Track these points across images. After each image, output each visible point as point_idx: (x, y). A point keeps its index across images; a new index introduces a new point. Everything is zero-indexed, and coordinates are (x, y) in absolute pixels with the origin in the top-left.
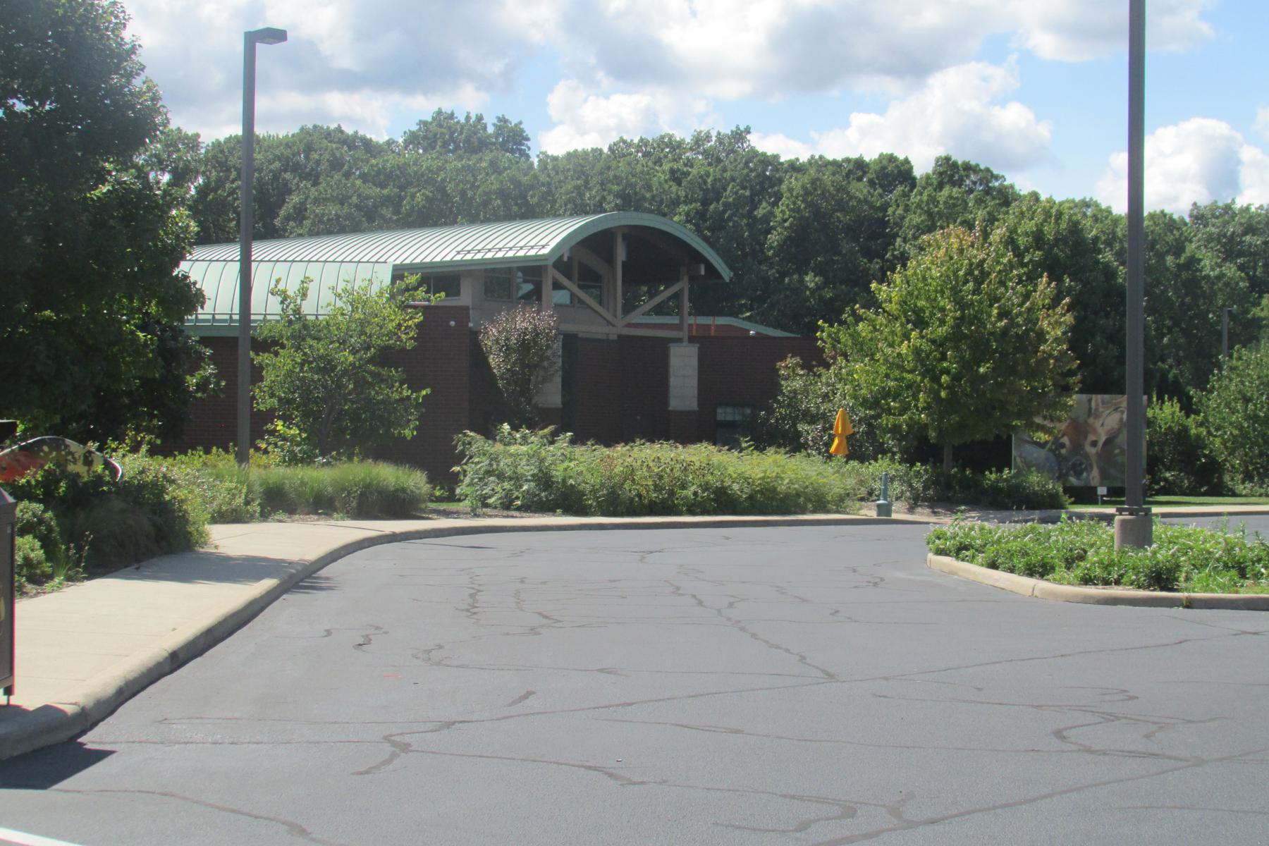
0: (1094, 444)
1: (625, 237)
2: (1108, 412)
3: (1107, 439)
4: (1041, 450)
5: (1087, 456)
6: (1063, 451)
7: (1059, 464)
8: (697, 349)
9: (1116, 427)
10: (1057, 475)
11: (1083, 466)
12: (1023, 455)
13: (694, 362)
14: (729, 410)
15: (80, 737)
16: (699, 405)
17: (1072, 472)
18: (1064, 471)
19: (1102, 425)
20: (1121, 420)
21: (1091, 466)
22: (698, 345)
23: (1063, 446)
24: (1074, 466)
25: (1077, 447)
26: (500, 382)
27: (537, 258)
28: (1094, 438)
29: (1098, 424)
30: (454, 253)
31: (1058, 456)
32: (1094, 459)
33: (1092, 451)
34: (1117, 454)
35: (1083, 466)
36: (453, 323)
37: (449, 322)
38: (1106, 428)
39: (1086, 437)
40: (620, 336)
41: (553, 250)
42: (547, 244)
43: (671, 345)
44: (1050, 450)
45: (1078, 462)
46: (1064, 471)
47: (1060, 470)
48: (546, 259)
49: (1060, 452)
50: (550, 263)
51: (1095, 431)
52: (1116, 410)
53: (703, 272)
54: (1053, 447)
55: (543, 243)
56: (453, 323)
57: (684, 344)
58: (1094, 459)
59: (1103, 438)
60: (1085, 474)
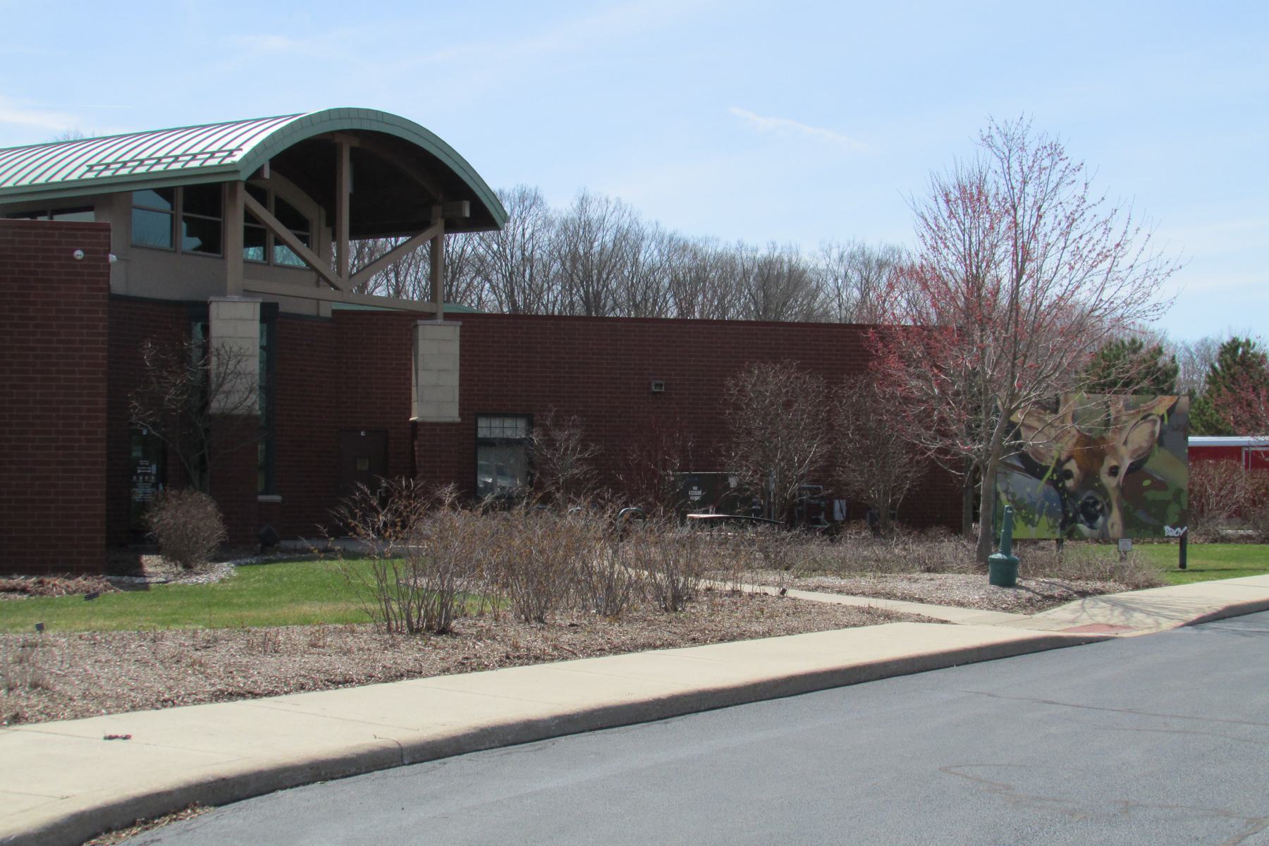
0: (1114, 471)
1: (356, 155)
2: (1134, 421)
3: (1131, 464)
4: (1034, 480)
5: (1102, 490)
6: (1069, 483)
7: (1063, 504)
8: (458, 329)
9: (1145, 445)
10: (1060, 521)
11: (1099, 507)
12: (1011, 489)
13: (454, 348)
14: (496, 423)
15: (421, 319)
16: (461, 415)
17: (1082, 517)
18: (1071, 515)
19: (1125, 443)
20: (1153, 433)
21: (1110, 506)
22: (460, 323)
23: (1069, 475)
24: (1085, 505)
25: (1090, 476)
26: (154, 472)
27: (221, 170)
28: (1114, 463)
29: (1117, 441)
30: (85, 168)
31: (1062, 491)
32: (1114, 496)
33: (1110, 482)
34: (1148, 488)
35: (1099, 507)
36: (79, 254)
37: (74, 250)
38: (1130, 447)
39: (1102, 461)
40: (334, 312)
41: (246, 158)
42: (239, 149)
43: (419, 322)
44: (1050, 481)
45: (1091, 501)
46: (1071, 515)
47: (1065, 513)
48: (236, 172)
49: (1064, 485)
50: (243, 176)
51: (1114, 450)
52: (1144, 418)
53: (467, 214)
54: (1055, 478)
55: (232, 146)
56: (79, 254)
57: (440, 321)
58: (1114, 496)
59: (1127, 463)
60: (1100, 519)
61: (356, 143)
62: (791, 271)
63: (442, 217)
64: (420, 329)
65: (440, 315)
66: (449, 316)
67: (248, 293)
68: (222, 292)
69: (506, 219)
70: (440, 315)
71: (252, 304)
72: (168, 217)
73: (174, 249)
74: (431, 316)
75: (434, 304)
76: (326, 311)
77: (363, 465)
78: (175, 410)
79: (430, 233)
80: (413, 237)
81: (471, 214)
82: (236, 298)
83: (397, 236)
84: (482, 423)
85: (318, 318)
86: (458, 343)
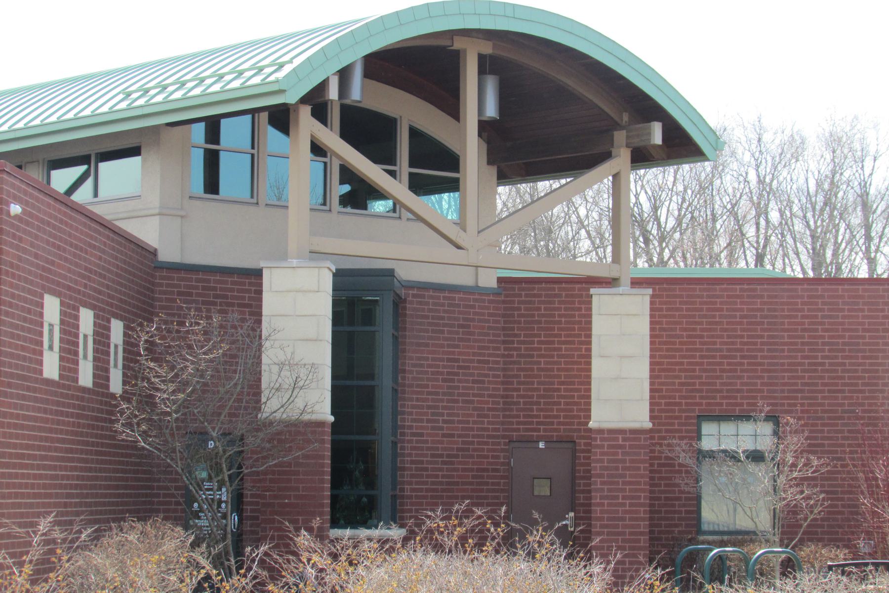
8: (647, 299)
13: (642, 326)
14: (728, 428)
16: (652, 418)
40: (500, 280)
42: (291, 61)
43: (593, 291)
61: (487, 48)
62: (490, 162)
63: (627, 146)
64: (595, 300)
65: (626, 281)
66: (637, 283)
67: (316, 255)
68: (282, 255)
69: (718, 143)
70: (626, 281)
71: (317, 270)
72: (248, 157)
73: (254, 201)
74: (610, 282)
75: (616, 266)
76: (488, 280)
77: (543, 489)
78: (169, 414)
79: (606, 169)
80: (576, 178)
81: (664, 140)
82: (295, 262)
83: (566, 178)
84: (708, 428)
85: (474, 291)
86: (647, 320)
